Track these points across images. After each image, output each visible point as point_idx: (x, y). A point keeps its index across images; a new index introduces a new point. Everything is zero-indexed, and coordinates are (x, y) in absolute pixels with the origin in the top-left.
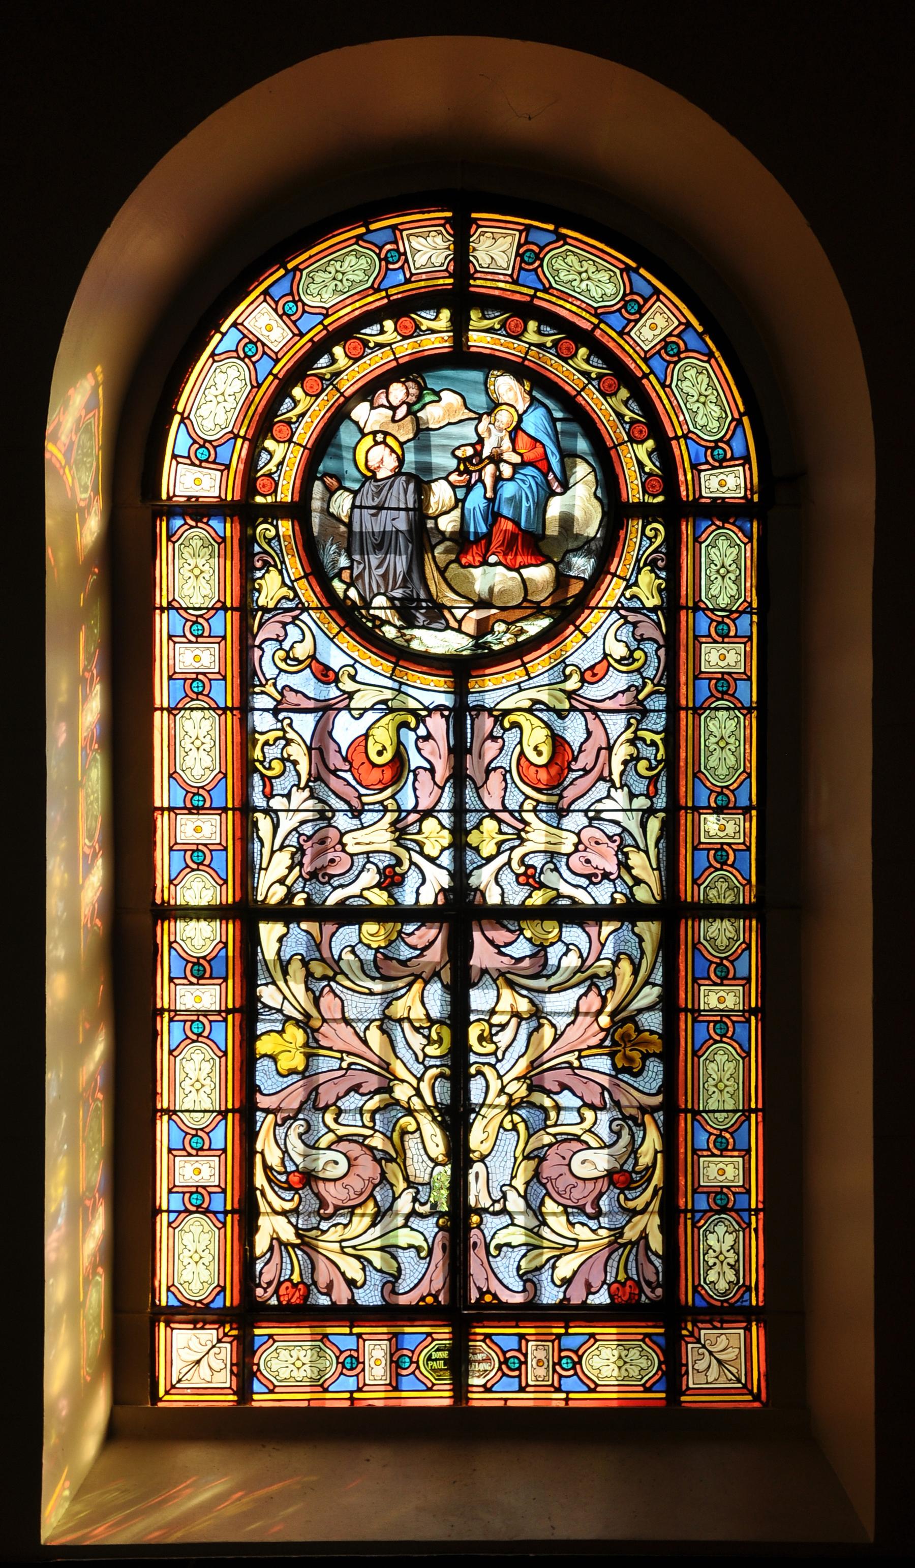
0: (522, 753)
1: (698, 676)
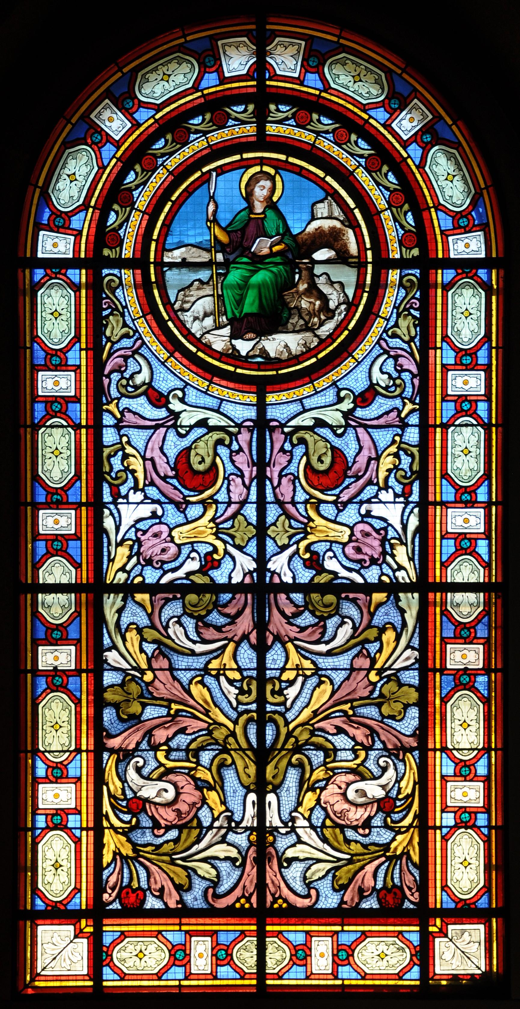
0: (308, 463)
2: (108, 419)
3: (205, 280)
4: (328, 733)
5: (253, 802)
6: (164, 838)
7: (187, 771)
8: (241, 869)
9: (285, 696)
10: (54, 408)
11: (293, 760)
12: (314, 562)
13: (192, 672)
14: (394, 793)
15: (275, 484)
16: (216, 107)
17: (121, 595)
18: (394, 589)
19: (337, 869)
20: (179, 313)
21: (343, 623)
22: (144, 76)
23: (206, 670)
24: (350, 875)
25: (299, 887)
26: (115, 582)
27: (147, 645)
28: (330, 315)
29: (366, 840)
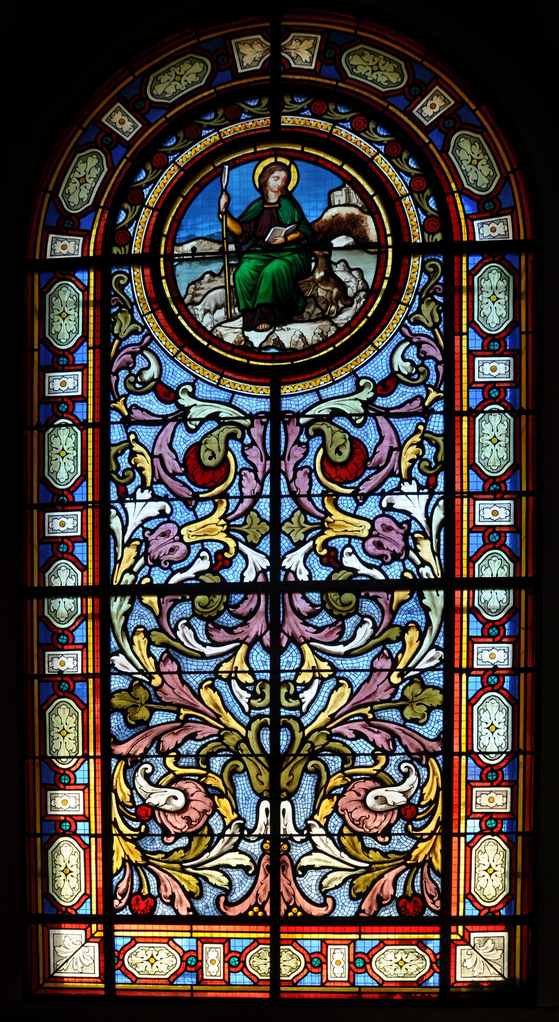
1: (472, 384)
2: (115, 417)
3: (216, 271)
4: (346, 738)
5: (267, 810)
6: (174, 846)
7: (197, 778)
8: (254, 877)
9: (300, 700)
10: (61, 408)
11: (309, 766)
12: (332, 559)
13: (202, 676)
14: (416, 800)
15: (290, 477)
16: (228, 103)
17: (128, 598)
18: (417, 586)
19: (355, 877)
20: (190, 307)
21: (362, 623)
22: (155, 78)
23: (216, 672)
24: (368, 884)
25: (315, 895)
26: (122, 583)
27: (155, 648)
28: (349, 302)
29: (386, 848)
